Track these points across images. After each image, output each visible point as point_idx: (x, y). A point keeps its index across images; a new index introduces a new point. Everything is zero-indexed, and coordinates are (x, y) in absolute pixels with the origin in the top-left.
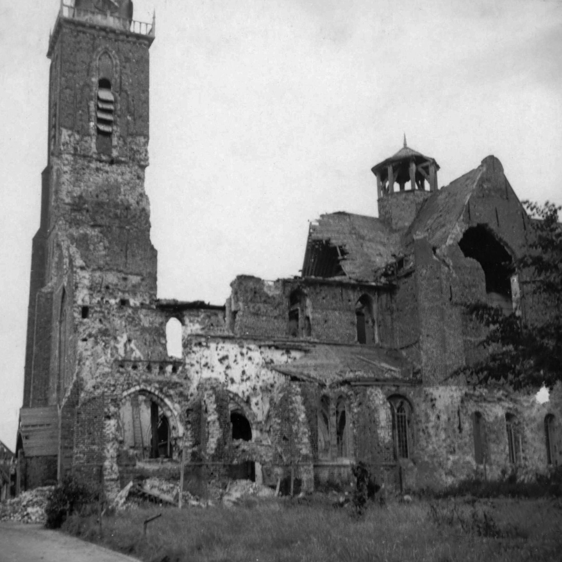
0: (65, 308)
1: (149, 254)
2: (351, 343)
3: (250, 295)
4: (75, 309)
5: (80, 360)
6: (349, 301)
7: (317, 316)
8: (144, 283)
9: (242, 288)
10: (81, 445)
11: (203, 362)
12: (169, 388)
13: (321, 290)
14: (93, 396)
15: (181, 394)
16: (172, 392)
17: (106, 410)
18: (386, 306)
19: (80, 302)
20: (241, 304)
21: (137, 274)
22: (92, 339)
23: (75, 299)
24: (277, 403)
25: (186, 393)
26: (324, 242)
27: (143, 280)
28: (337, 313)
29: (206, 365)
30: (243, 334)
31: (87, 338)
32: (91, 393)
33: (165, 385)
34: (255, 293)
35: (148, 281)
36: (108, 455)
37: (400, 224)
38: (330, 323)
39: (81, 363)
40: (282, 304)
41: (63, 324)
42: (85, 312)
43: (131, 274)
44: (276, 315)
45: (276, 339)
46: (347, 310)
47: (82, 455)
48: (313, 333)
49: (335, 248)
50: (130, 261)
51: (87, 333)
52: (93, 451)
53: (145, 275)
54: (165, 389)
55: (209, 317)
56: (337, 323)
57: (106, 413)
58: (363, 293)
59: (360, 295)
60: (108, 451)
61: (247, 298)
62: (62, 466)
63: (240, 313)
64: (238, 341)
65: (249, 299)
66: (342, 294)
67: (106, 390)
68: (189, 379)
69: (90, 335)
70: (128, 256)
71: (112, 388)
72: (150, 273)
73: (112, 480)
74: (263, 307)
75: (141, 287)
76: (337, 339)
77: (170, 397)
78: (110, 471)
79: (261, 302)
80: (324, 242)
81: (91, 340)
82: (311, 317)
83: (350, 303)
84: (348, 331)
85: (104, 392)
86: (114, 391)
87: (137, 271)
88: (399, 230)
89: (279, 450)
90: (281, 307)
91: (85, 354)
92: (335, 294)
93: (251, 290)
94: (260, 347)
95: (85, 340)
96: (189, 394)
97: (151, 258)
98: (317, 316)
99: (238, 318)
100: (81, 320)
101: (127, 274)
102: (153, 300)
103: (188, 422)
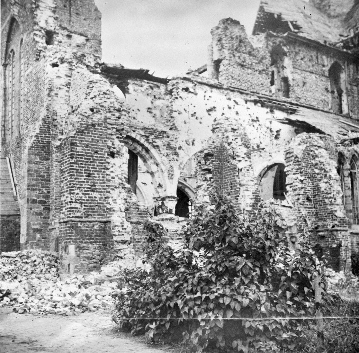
0: (13, 47)
1: (93, 15)
2: (326, 109)
3: (236, 43)
4: (37, 32)
5: (51, 90)
6: (324, 66)
7: (296, 76)
8: (88, 44)
9: (228, 33)
10: (77, 191)
11: (191, 111)
12: (157, 137)
13: (300, 50)
14: (90, 121)
15: (169, 146)
16: (159, 142)
17: (110, 144)
18: (353, 77)
19: (42, 24)
20: (226, 52)
21: (81, 34)
22: (66, 64)
23: (37, 20)
24: (300, 156)
25: (173, 144)
26: (276, 16)
27: (87, 40)
28: (313, 76)
29: (194, 115)
30: (229, 85)
31: (59, 63)
32: (87, 117)
33: (151, 134)
34: (241, 41)
35: (92, 42)
36: (116, 207)
37: (339, 10)
38: (308, 85)
39: (53, 93)
40: (266, 58)
41: (9, 68)
42: (49, 37)
43: (75, 33)
44: (260, 69)
45: (260, 95)
46: (322, 75)
47: (78, 206)
48: (292, 95)
49: (287, 22)
50: (74, 18)
51: (58, 55)
52: (93, 200)
53: (89, 36)
54: (151, 137)
55: (152, 88)
56: (314, 87)
57: (109, 147)
58: (335, 60)
59: (333, 62)
60: (114, 201)
61: (233, 46)
62: (28, 225)
63: (225, 62)
64: (226, 92)
65: (235, 47)
66: (317, 58)
67: (109, 115)
68: (176, 129)
69: (62, 61)
70: (72, 14)
71: (117, 114)
72: (94, 35)
73: (124, 242)
74: (249, 60)
75: (86, 47)
76: (314, 104)
77: (156, 147)
78: (120, 229)
79: (246, 53)
80: (276, 16)
81: (63, 68)
82: (290, 78)
83: (324, 69)
84: (323, 97)
85: (106, 118)
86: (119, 118)
87: (81, 31)
88: (337, 16)
89: (304, 212)
90: (264, 61)
91: (58, 82)
92: (311, 57)
93: (237, 38)
94: (246, 102)
95: (55, 65)
96: (177, 147)
97: (95, 20)
98: (296, 76)
99: (222, 68)
100: (45, 45)
101: (71, 32)
102: (98, 63)
103: (209, 171)
